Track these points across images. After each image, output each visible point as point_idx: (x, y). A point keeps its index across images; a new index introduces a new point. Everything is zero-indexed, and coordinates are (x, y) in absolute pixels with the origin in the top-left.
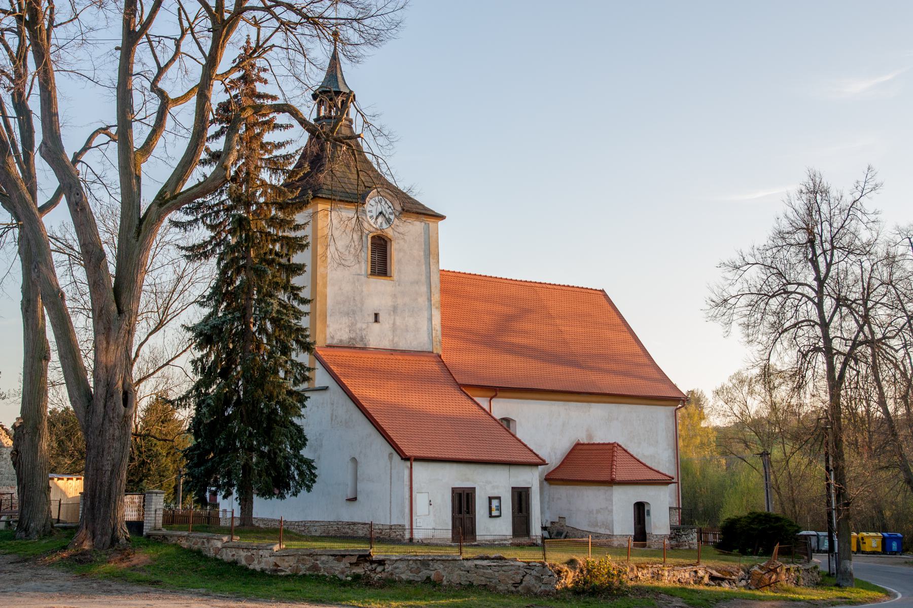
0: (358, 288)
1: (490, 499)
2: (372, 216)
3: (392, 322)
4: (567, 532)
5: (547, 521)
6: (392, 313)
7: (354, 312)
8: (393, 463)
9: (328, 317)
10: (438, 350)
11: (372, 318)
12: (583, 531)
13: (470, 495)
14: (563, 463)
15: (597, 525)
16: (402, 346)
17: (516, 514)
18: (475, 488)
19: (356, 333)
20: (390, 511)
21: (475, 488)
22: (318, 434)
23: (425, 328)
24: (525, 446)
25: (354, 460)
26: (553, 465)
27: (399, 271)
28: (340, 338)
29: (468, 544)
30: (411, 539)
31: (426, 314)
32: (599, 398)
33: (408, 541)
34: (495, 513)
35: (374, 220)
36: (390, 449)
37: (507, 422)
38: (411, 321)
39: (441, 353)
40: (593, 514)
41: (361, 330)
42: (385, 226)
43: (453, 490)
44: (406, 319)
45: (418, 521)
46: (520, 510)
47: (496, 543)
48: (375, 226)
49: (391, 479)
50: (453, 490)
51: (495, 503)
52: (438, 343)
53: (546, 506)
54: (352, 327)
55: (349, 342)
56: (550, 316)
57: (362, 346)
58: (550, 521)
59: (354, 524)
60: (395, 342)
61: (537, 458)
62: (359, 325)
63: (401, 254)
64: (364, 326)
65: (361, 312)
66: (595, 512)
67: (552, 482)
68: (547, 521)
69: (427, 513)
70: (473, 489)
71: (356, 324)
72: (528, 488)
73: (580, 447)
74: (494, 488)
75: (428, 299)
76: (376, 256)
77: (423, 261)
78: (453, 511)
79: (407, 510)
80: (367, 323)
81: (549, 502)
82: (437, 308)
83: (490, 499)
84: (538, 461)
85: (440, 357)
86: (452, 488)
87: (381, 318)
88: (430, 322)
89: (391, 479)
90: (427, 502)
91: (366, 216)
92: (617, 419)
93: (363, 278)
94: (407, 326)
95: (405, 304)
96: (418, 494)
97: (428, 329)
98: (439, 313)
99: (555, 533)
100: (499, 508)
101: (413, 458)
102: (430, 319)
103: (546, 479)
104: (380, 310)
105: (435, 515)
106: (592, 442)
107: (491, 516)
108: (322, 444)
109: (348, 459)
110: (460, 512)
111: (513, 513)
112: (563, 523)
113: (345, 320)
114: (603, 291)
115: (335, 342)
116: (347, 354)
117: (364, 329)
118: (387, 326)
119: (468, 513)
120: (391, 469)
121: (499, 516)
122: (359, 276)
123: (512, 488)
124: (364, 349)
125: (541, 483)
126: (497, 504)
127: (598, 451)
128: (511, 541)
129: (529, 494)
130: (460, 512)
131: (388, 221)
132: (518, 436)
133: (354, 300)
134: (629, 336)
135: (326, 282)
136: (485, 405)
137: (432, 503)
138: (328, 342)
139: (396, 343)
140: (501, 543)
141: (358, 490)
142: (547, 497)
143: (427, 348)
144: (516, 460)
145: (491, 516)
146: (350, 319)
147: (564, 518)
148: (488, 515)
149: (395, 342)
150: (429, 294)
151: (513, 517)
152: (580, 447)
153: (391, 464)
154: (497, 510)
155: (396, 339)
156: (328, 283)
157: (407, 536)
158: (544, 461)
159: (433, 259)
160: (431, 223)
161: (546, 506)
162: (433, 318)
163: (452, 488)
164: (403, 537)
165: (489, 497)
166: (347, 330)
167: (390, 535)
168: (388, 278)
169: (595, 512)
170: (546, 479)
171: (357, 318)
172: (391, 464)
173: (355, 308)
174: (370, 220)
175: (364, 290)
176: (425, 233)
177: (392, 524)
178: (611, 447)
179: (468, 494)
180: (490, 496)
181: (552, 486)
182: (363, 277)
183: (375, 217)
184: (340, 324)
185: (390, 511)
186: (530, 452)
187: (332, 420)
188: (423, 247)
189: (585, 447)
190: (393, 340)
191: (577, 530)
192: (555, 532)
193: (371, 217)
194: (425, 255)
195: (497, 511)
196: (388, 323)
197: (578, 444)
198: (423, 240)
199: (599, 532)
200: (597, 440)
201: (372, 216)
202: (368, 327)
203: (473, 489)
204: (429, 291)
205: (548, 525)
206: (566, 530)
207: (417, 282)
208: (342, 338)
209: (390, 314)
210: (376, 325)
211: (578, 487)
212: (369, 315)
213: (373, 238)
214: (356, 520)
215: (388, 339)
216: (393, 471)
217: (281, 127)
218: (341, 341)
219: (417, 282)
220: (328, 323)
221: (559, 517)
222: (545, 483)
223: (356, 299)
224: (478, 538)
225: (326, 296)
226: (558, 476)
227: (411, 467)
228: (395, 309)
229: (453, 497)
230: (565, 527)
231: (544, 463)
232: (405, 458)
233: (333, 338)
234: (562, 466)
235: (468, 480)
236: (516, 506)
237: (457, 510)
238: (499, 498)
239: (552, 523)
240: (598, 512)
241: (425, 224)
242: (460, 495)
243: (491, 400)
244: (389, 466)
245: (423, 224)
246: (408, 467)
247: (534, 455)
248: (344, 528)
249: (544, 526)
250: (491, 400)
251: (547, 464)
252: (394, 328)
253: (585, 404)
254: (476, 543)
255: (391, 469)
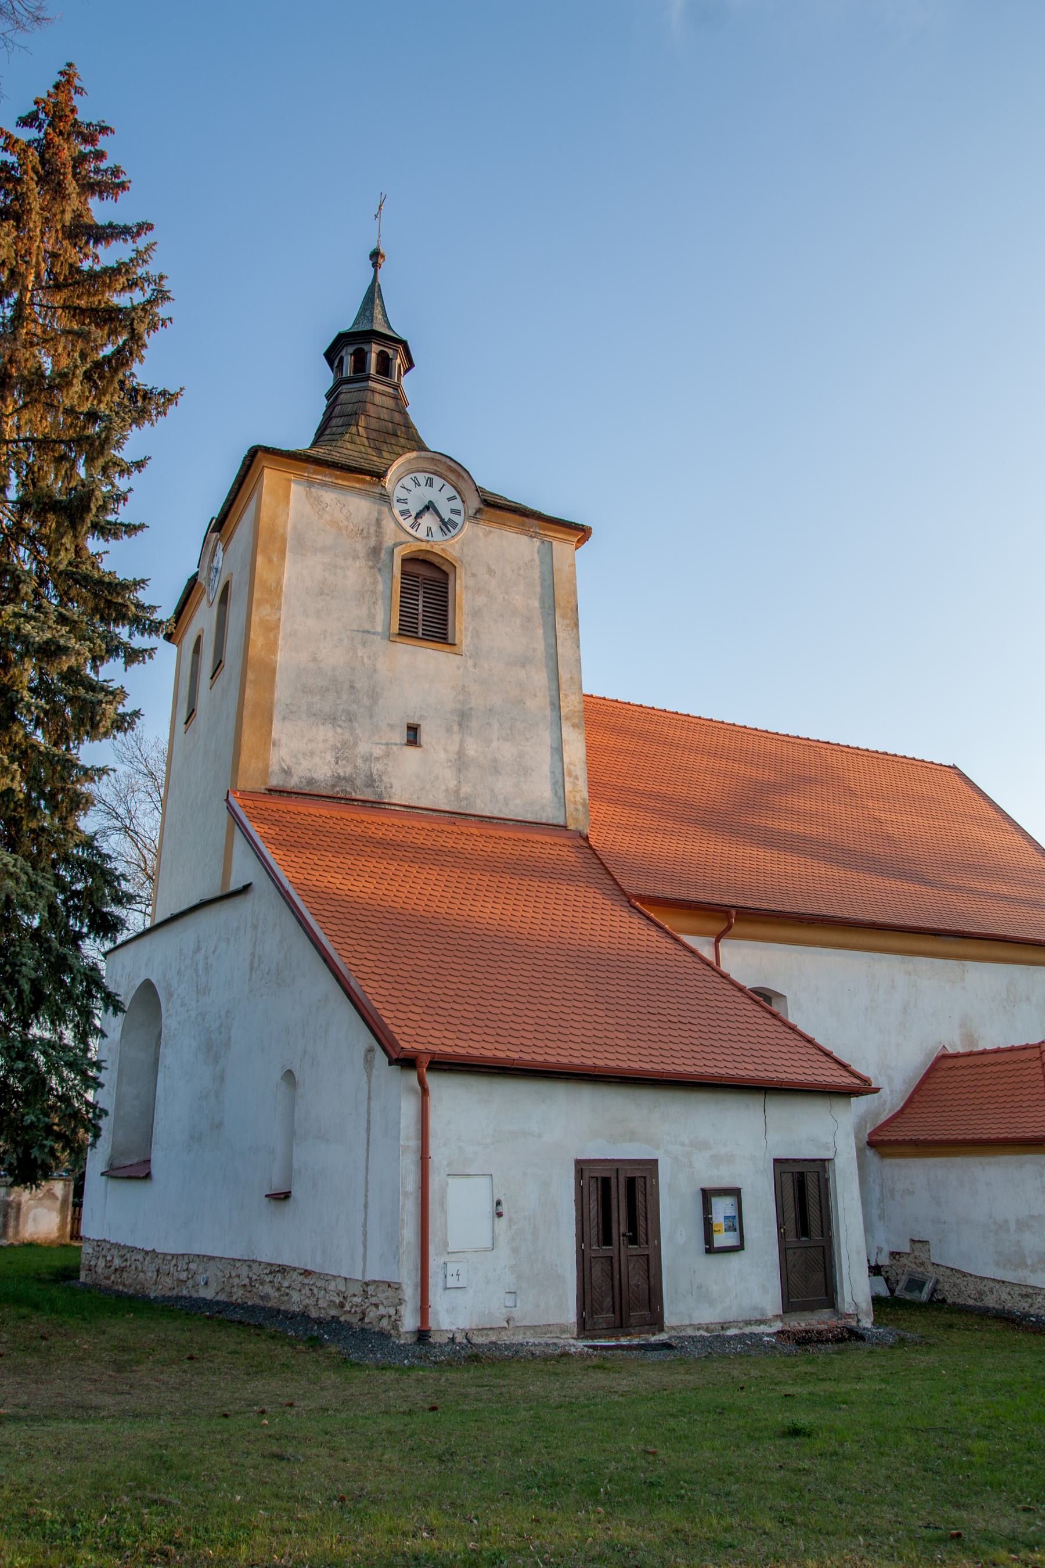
0: (363, 663)
1: (707, 1195)
2: (408, 511)
3: (455, 748)
4: (937, 1281)
5: (880, 1250)
6: (456, 728)
7: (351, 717)
8: (373, 1079)
9: (274, 722)
10: (579, 822)
11: (400, 736)
12: (982, 1278)
13: (639, 1183)
14: (910, 1102)
15: (1022, 1264)
16: (484, 807)
17: (791, 1238)
18: (655, 1162)
19: (356, 767)
20: (365, 1234)
21: (655, 1162)
22: (223, 1014)
23: (546, 769)
24: (810, 1041)
25: (289, 1075)
26: (888, 1107)
27: (476, 634)
28: (308, 775)
29: (635, 1341)
30: (422, 1335)
31: (546, 737)
32: (983, 949)
33: (411, 1340)
34: (723, 1238)
35: (411, 520)
36: (366, 1039)
37: (763, 998)
38: (507, 752)
39: (587, 831)
40: (1008, 1231)
41: (368, 758)
42: (438, 536)
43: (581, 1167)
44: (495, 744)
45: (452, 1269)
46: (803, 1229)
47: (731, 1332)
48: (412, 532)
49: (368, 1129)
50: (581, 1167)
51: (722, 1208)
52: (580, 807)
53: (875, 1212)
54: (342, 752)
55: (334, 786)
56: (851, 792)
57: (371, 799)
58: (887, 1249)
59: (283, 1270)
60: (462, 795)
61: (846, 1074)
62: (363, 748)
63: (481, 600)
64: (378, 751)
65: (371, 717)
66: (1012, 1227)
67: (888, 1150)
68: (880, 1250)
69: (490, 1245)
70: (652, 1165)
71: (356, 744)
72: (824, 1160)
73: (950, 1063)
74: (716, 1160)
75: (552, 704)
76: (421, 603)
77: (538, 619)
78: (581, 1237)
79: (409, 1234)
80: (387, 744)
81: (881, 1201)
82: (574, 726)
83: (707, 1195)
84: (849, 1081)
85: (586, 839)
86: (578, 1162)
87: (424, 737)
88: (557, 757)
89: (368, 1129)
90: (488, 1207)
91: (391, 509)
92: (1028, 999)
93: (379, 643)
94: (495, 760)
95: (490, 710)
96: (450, 1180)
97: (553, 773)
98: (582, 737)
99: (902, 1284)
100: (737, 1224)
101: (425, 1060)
102: (558, 750)
103: (871, 1144)
104: (421, 717)
105: (515, 1251)
106: (980, 1048)
107: (710, 1249)
108: (229, 1038)
109: (277, 1075)
110: (606, 1239)
111: (782, 1237)
112: (923, 1256)
113: (325, 735)
114: (954, 767)
115: (293, 783)
116: (324, 812)
117: (377, 759)
118: (442, 755)
119: (633, 1240)
120: (369, 1098)
121: (739, 1248)
122: (365, 635)
123: (776, 1161)
124: (376, 805)
125: (860, 1152)
126: (731, 1212)
127: (999, 1068)
128: (778, 1326)
129: (827, 1180)
130: (606, 1239)
131: (446, 525)
132: (791, 1020)
133: (352, 687)
134: (1018, 838)
135: (276, 639)
136: (706, 951)
137: (504, 1209)
138: (274, 782)
139: (466, 798)
140: (747, 1330)
141: (295, 1166)
142: (877, 1188)
143: (550, 814)
144: (783, 1076)
145: (710, 1249)
146: (339, 730)
147: (926, 1242)
148: (702, 1246)
149: (462, 795)
150: (554, 693)
151: (783, 1250)
152: (950, 1063)
153: (369, 1081)
154: (728, 1229)
155: (466, 789)
156: (280, 642)
157: (409, 1322)
158: (866, 1081)
159: (563, 617)
160: (562, 548)
161: (875, 1212)
162: (566, 748)
163: (578, 1162)
164: (395, 1327)
165: (704, 1191)
166: (330, 757)
167: (364, 1313)
168: (447, 648)
169: (1012, 1227)
170: (871, 1144)
171: (358, 731)
172: (369, 1081)
173: (355, 707)
174: (400, 519)
175: (379, 666)
176: (542, 563)
177: (369, 1278)
178: (1036, 1053)
179: (631, 1182)
180: (707, 1185)
181: (888, 1161)
182: (379, 638)
183: (414, 514)
184: (311, 741)
185: (365, 1234)
186: (824, 1059)
187: (251, 969)
188: (538, 589)
189: (962, 1062)
190: (457, 792)
191: (965, 1275)
192: (904, 1280)
193: (403, 513)
194: (542, 607)
195: (731, 1234)
196: (446, 750)
197: (944, 1057)
198: (537, 575)
199: (1029, 1282)
200: (988, 1043)
201: (408, 511)
202: (387, 755)
203: (652, 1165)
204: (554, 687)
205: (884, 1260)
206: (932, 1274)
207: (524, 662)
208: (315, 776)
209: (449, 730)
210: (411, 751)
211: (958, 1160)
212: (392, 727)
213: (405, 561)
214: (286, 1259)
215: (443, 788)
216: (373, 1103)
217: (123, 233)
218: (311, 781)
219: (524, 662)
220: (275, 735)
221: (913, 1241)
222: (870, 1153)
223: (358, 686)
224: (670, 1319)
225: (274, 672)
226: (886, 1136)
227: (425, 1092)
228: (463, 717)
229: (580, 1191)
230: (930, 1268)
231: (863, 1088)
232: (406, 1062)
233: (287, 772)
234: (908, 1110)
235: (632, 1136)
236: (791, 1215)
237: (594, 1231)
238: (735, 1193)
239: (894, 1255)
240: (1022, 1225)
241: (543, 542)
242: (606, 1182)
243: (717, 941)
244: (366, 1087)
245: (537, 542)
246: (412, 1090)
247: (835, 1066)
248: (262, 1283)
249: (873, 1264)
250: (717, 941)
251: (877, 1090)
252: (461, 763)
253: (952, 963)
254: (663, 1337)
255: (369, 1098)
